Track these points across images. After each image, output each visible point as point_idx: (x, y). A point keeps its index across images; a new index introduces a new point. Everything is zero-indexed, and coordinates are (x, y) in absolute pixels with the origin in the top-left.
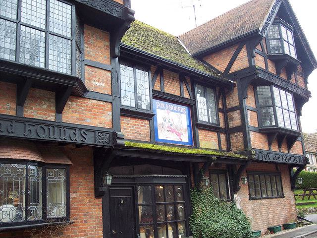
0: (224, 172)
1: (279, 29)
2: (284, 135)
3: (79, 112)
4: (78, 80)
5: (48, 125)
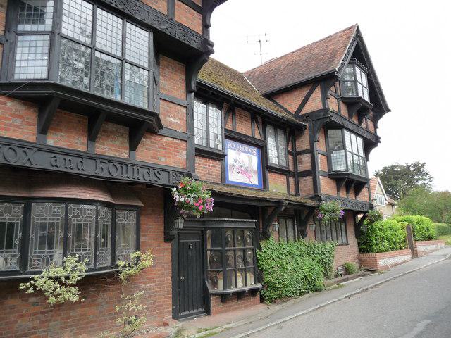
0: (292, 217)
1: (354, 70)
2: (353, 180)
3: (154, 150)
4: (155, 115)
5: (120, 163)
